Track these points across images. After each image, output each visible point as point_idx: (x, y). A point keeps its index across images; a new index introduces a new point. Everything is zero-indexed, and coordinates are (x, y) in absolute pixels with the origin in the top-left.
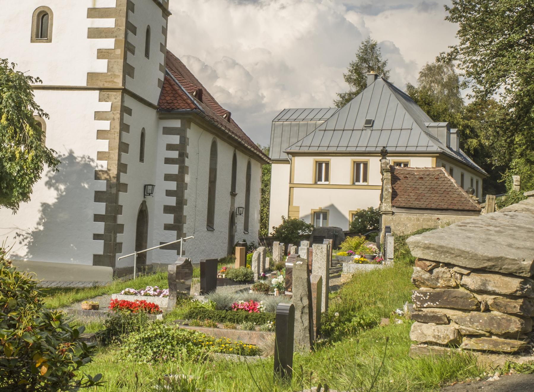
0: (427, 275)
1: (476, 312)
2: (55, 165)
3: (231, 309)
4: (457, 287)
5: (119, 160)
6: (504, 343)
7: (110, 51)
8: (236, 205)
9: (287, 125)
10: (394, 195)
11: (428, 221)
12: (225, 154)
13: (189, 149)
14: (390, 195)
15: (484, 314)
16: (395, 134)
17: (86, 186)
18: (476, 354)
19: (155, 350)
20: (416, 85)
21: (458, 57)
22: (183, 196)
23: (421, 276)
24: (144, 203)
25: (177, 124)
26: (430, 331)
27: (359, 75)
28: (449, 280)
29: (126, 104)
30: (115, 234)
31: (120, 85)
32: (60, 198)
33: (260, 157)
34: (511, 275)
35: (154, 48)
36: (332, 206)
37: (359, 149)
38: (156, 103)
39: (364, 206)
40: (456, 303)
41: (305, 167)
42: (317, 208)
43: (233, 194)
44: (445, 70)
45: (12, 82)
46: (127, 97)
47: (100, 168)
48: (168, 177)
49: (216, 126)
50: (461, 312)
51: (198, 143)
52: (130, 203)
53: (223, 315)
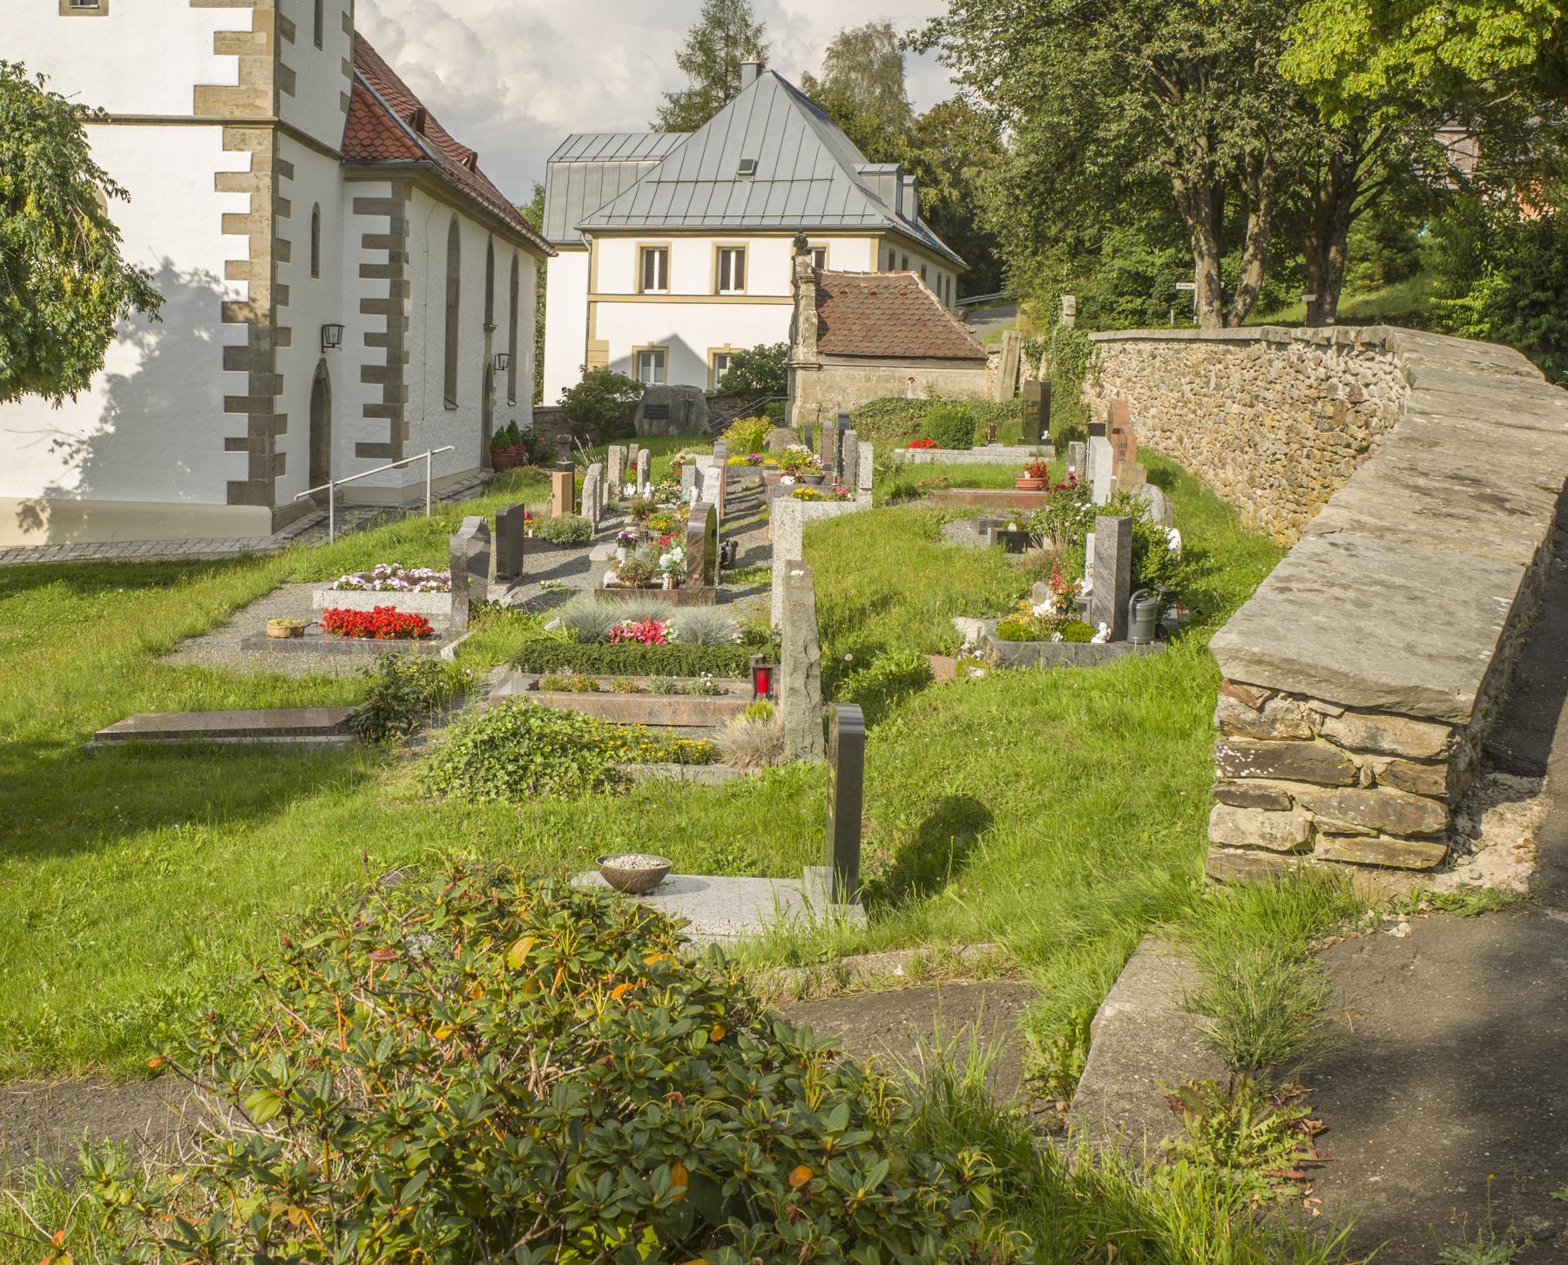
0: (1251, 715)
1: (1350, 790)
2: (154, 306)
3: (608, 639)
4: (1312, 738)
5: (273, 278)
6: (1409, 852)
7: (242, 37)
8: (495, 351)
9: (578, 170)
10: (822, 329)
11: (888, 381)
12: (473, 242)
13: (410, 245)
14: (814, 330)
15: (1368, 793)
16: (800, 190)
17: (205, 336)
18: (1348, 870)
19: (510, 768)
20: (820, 75)
21: (941, 41)
22: (400, 345)
23: (1237, 717)
24: (322, 365)
25: (383, 190)
26: (1252, 823)
27: (706, 54)
28: (1298, 725)
29: (282, 156)
30: (272, 436)
31: (269, 114)
32: (149, 363)
33: (536, 245)
34: (1431, 719)
35: (332, 23)
36: (675, 339)
37: (728, 222)
38: (336, 146)
39: (745, 342)
40: (1312, 771)
41: (618, 260)
42: (643, 342)
43: (489, 328)
44: (877, 44)
45: (44, 118)
46: (284, 140)
47: (232, 297)
48: (368, 306)
49: (460, 191)
50: (1316, 788)
51: (426, 224)
52: (296, 365)
53: (596, 655)
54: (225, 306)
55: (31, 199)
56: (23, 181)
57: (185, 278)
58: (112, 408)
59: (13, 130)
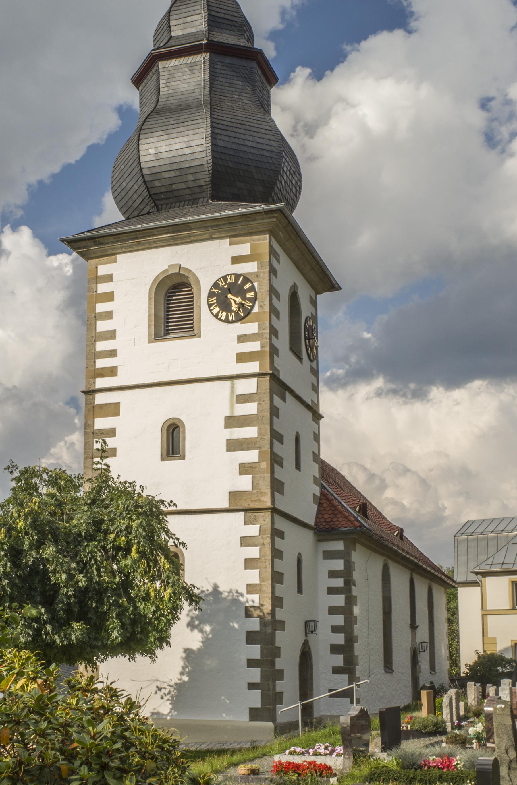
3: (420, 767)
5: (273, 592)
7: (254, 465)
8: (418, 640)
9: (473, 540)
13: (356, 576)
17: (236, 626)
22: (352, 631)
24: (306, 644)
25: (339, 546)
29: (277, 526)
30: (274, 681)
31: (269, 505)
32: (206, 642)
35: (306, 458)
38: (312, 523)
43: (413, 626)
46: (277, 518)
47: (251, 604)
48: (333, 610)
52: (289, 642)
53: (412, 776)
54: (247, 609)
55: (134, 549)
56: (131, 540)
57: (225, 595)
58: (187, 667)
59: (127, 514)
